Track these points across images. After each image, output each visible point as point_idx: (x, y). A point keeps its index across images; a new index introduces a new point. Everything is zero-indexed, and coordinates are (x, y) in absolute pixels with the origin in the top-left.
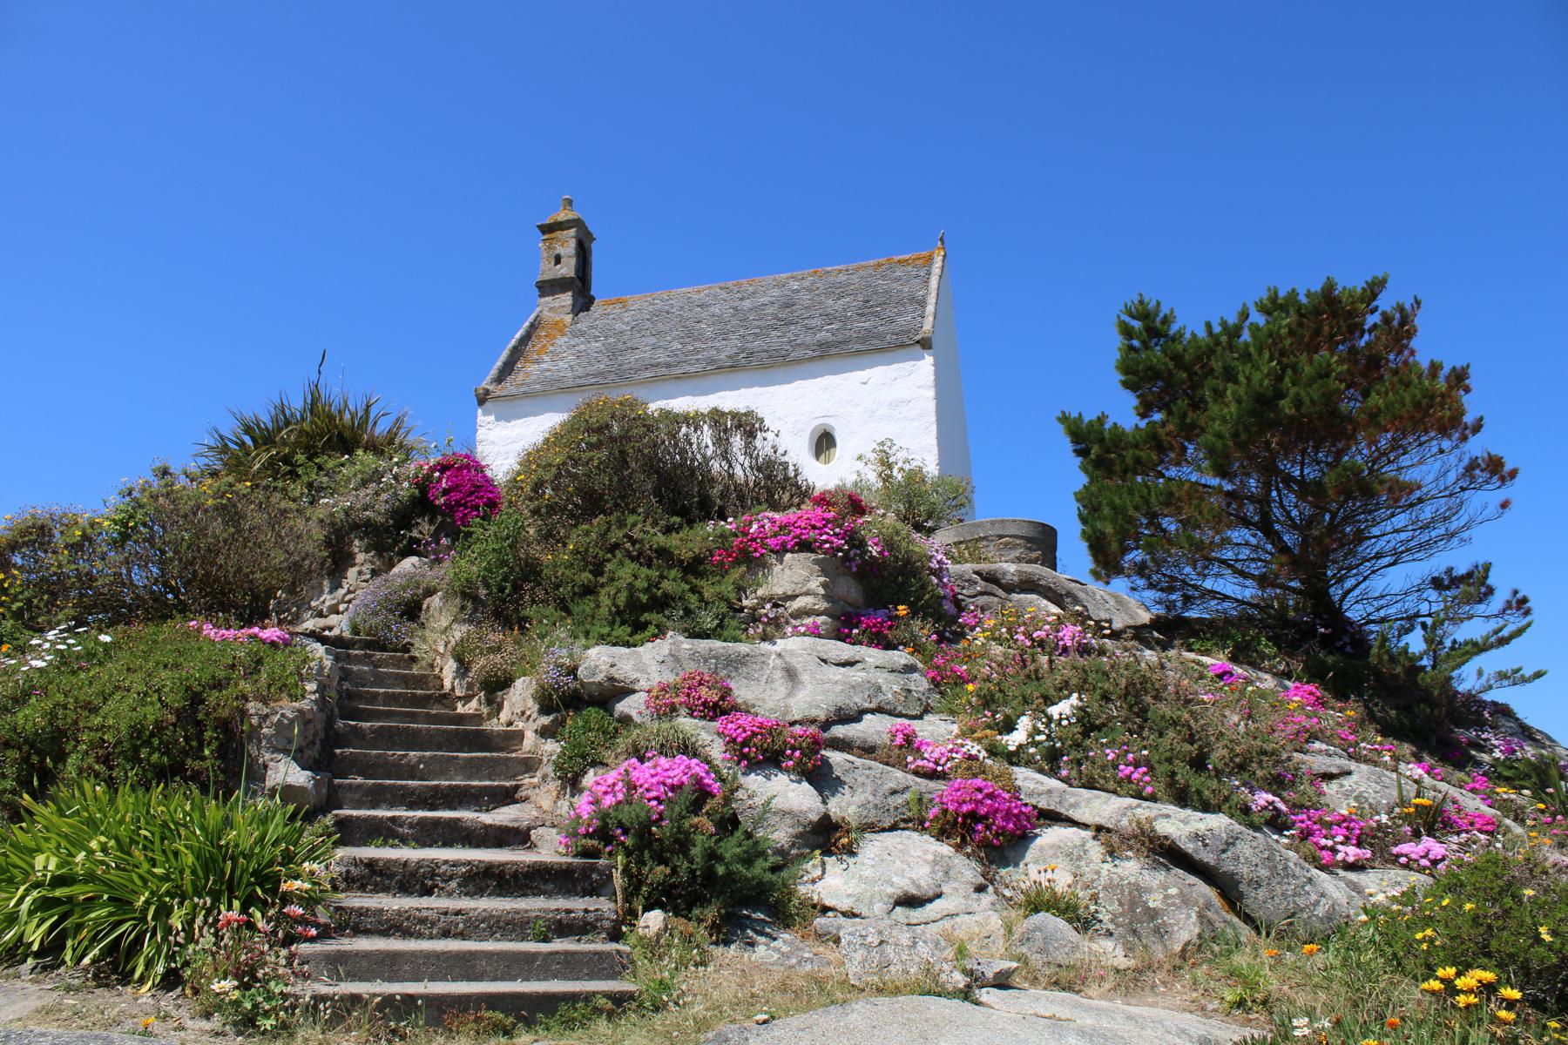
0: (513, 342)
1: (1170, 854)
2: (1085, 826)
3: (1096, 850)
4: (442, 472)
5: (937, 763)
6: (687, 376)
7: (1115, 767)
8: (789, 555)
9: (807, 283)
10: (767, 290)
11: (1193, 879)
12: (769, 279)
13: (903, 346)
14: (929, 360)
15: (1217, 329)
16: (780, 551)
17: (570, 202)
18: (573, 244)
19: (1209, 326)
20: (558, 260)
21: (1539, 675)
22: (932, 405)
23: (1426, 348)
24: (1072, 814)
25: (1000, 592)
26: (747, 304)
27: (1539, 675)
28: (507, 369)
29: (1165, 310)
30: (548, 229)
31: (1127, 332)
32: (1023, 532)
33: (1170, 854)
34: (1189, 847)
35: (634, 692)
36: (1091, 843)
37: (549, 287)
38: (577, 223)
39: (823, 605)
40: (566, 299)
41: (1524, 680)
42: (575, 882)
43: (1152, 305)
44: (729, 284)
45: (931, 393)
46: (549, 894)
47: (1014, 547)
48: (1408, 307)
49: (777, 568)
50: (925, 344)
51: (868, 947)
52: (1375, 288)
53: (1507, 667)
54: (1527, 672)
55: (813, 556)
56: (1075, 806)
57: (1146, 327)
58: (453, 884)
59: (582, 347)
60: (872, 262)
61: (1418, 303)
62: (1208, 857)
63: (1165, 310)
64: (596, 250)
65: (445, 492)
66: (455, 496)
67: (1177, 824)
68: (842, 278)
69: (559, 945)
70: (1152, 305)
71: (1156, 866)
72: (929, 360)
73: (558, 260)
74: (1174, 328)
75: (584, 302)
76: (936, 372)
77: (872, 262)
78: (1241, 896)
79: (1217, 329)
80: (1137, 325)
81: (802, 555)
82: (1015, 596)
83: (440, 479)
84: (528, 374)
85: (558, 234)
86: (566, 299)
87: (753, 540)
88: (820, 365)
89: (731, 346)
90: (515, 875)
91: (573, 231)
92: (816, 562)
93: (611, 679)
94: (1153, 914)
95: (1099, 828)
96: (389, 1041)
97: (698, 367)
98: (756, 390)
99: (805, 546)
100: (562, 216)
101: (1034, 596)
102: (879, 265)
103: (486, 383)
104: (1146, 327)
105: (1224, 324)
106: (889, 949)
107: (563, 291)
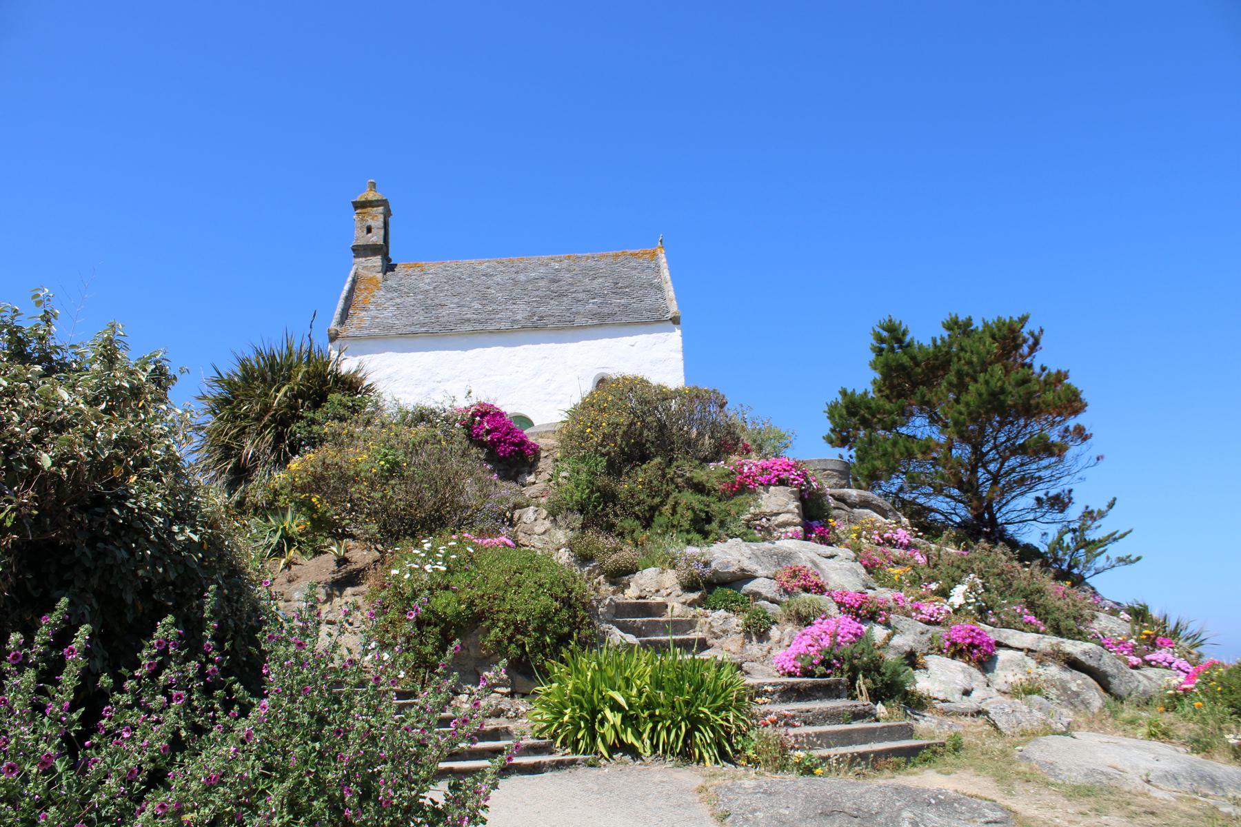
0: (344, 293)
1: (1073, 664)
2: (1021, 650)
3: (1031, 663)
4: (482, 417)
5: (931, 616)
6: (499, 331)
7: (1021, 616)
8: (772, 488)
9: (565, 264)
10: (536, 266)
11: (1084, 675)
12: (535, 259)
13: (659, 321)
14: (678, 332)
15: (939, 342)
16: (769, 484)
17: (374, 185)
18: (381, 218)
19: (934, 340)
20: (369, 230)
21: (1138, 559)
22: (681, 365)
23: (1046, 359)
24: (1007, 642)
25: (846, 507)
26: (522, 277)
27: (1138, 559)
28: (345, 315)
29: (903, 327)
30: (360, 205)
31: (881, 340)
32: (837, 468)
33: (1073, 664)
34: (1083, 658)
35: (755, 577)
36: (1027, 659)
37: (362, 251)
38: (384, 203)
39: (798, 520)
40: (377, 261)
41: (1131, 562)
42: (832, 690)
43: (897, 322)
44: (504, 259)
45: (680, 356)
46: (820, 699)
47: (833, 477)
48: (1036, 333)
49: (765, 496)
50: (675, 321)
51: (1007, 714)
52: (1023, 320)
53: (1123, 555)
54: (1133, 558)
55: (790, 489)
56: (1007, 638)
57: (892, 337)
58: (776, 696)
59: (398, 301)
60: (611, 253)
61: (1042, 331)
62: (1093, 663)
63: (903, 327)
64: (391, 220)
65: (488, 432)
66: (497, 435)
67: (1073, 647)
68: (591, 263)
69: (856, 725)
70: (897, 322)
71: (1065, 670)
72: (678, 332)
73: (369, 230)
74: (907, 339)
75: (389, 267)
76: (684, 342)
77: (611, 253)
78: (1109, 683)
79: (939, 342)
80: (885, 334)
81: (782, 488)
82: (856, 510)
83: (481, 423)
84: (361, 320)
85: (369, 209)
86: (377, 261)
87: (748, 477)
88: (599, 330)
89: (521, 312)
90: (805, 690)
91: (381, 209)
92: (792, 492)
93: (743, 570)
94: (1077, 694)
95: (1029, 650)
96: (431, 824)
97: (508, 325)
98: (552, 345)
99: (782, 482)
100: (371, 196)
101: (868, 511)
102: (617, 256)
103: (333, 325)
104: (892, 337)
105: (942, 339)
106: (1018, 714)
107: (374, 254)
